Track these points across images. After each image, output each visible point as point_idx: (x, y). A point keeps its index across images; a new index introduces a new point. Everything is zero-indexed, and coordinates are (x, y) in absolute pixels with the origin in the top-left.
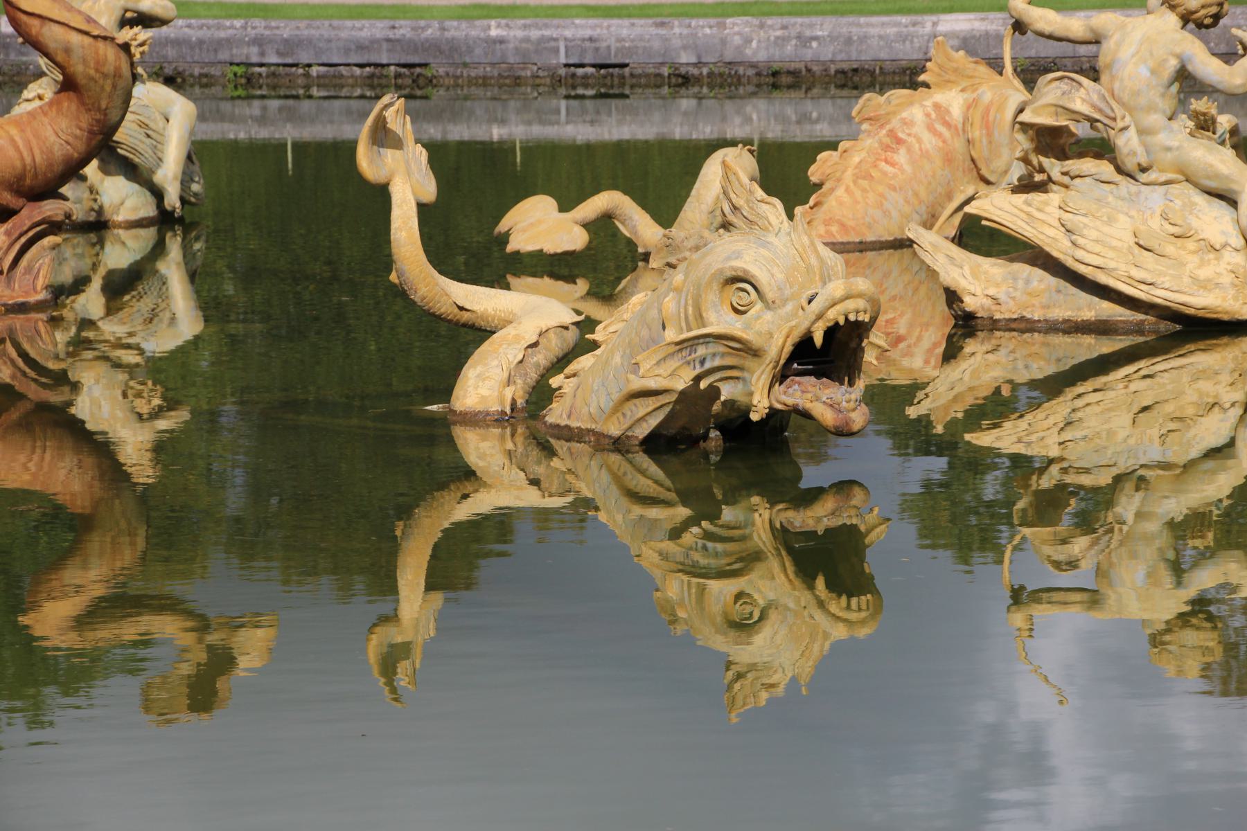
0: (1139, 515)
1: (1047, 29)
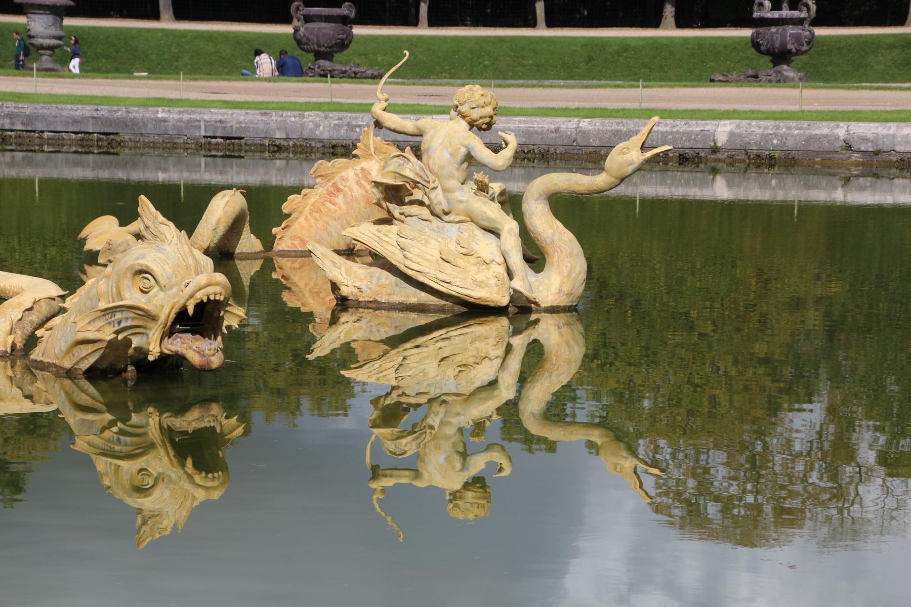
0: (442, 423)
1: (393, 126)
